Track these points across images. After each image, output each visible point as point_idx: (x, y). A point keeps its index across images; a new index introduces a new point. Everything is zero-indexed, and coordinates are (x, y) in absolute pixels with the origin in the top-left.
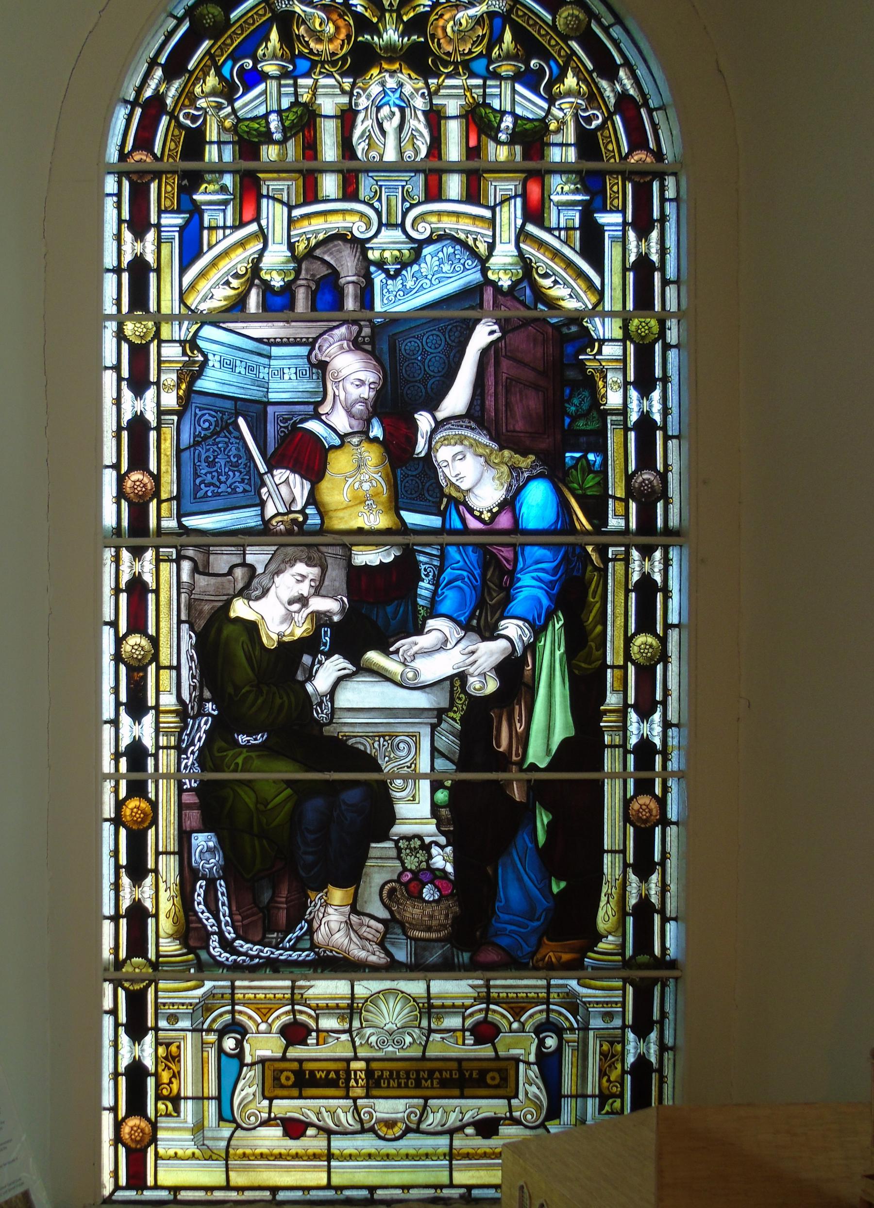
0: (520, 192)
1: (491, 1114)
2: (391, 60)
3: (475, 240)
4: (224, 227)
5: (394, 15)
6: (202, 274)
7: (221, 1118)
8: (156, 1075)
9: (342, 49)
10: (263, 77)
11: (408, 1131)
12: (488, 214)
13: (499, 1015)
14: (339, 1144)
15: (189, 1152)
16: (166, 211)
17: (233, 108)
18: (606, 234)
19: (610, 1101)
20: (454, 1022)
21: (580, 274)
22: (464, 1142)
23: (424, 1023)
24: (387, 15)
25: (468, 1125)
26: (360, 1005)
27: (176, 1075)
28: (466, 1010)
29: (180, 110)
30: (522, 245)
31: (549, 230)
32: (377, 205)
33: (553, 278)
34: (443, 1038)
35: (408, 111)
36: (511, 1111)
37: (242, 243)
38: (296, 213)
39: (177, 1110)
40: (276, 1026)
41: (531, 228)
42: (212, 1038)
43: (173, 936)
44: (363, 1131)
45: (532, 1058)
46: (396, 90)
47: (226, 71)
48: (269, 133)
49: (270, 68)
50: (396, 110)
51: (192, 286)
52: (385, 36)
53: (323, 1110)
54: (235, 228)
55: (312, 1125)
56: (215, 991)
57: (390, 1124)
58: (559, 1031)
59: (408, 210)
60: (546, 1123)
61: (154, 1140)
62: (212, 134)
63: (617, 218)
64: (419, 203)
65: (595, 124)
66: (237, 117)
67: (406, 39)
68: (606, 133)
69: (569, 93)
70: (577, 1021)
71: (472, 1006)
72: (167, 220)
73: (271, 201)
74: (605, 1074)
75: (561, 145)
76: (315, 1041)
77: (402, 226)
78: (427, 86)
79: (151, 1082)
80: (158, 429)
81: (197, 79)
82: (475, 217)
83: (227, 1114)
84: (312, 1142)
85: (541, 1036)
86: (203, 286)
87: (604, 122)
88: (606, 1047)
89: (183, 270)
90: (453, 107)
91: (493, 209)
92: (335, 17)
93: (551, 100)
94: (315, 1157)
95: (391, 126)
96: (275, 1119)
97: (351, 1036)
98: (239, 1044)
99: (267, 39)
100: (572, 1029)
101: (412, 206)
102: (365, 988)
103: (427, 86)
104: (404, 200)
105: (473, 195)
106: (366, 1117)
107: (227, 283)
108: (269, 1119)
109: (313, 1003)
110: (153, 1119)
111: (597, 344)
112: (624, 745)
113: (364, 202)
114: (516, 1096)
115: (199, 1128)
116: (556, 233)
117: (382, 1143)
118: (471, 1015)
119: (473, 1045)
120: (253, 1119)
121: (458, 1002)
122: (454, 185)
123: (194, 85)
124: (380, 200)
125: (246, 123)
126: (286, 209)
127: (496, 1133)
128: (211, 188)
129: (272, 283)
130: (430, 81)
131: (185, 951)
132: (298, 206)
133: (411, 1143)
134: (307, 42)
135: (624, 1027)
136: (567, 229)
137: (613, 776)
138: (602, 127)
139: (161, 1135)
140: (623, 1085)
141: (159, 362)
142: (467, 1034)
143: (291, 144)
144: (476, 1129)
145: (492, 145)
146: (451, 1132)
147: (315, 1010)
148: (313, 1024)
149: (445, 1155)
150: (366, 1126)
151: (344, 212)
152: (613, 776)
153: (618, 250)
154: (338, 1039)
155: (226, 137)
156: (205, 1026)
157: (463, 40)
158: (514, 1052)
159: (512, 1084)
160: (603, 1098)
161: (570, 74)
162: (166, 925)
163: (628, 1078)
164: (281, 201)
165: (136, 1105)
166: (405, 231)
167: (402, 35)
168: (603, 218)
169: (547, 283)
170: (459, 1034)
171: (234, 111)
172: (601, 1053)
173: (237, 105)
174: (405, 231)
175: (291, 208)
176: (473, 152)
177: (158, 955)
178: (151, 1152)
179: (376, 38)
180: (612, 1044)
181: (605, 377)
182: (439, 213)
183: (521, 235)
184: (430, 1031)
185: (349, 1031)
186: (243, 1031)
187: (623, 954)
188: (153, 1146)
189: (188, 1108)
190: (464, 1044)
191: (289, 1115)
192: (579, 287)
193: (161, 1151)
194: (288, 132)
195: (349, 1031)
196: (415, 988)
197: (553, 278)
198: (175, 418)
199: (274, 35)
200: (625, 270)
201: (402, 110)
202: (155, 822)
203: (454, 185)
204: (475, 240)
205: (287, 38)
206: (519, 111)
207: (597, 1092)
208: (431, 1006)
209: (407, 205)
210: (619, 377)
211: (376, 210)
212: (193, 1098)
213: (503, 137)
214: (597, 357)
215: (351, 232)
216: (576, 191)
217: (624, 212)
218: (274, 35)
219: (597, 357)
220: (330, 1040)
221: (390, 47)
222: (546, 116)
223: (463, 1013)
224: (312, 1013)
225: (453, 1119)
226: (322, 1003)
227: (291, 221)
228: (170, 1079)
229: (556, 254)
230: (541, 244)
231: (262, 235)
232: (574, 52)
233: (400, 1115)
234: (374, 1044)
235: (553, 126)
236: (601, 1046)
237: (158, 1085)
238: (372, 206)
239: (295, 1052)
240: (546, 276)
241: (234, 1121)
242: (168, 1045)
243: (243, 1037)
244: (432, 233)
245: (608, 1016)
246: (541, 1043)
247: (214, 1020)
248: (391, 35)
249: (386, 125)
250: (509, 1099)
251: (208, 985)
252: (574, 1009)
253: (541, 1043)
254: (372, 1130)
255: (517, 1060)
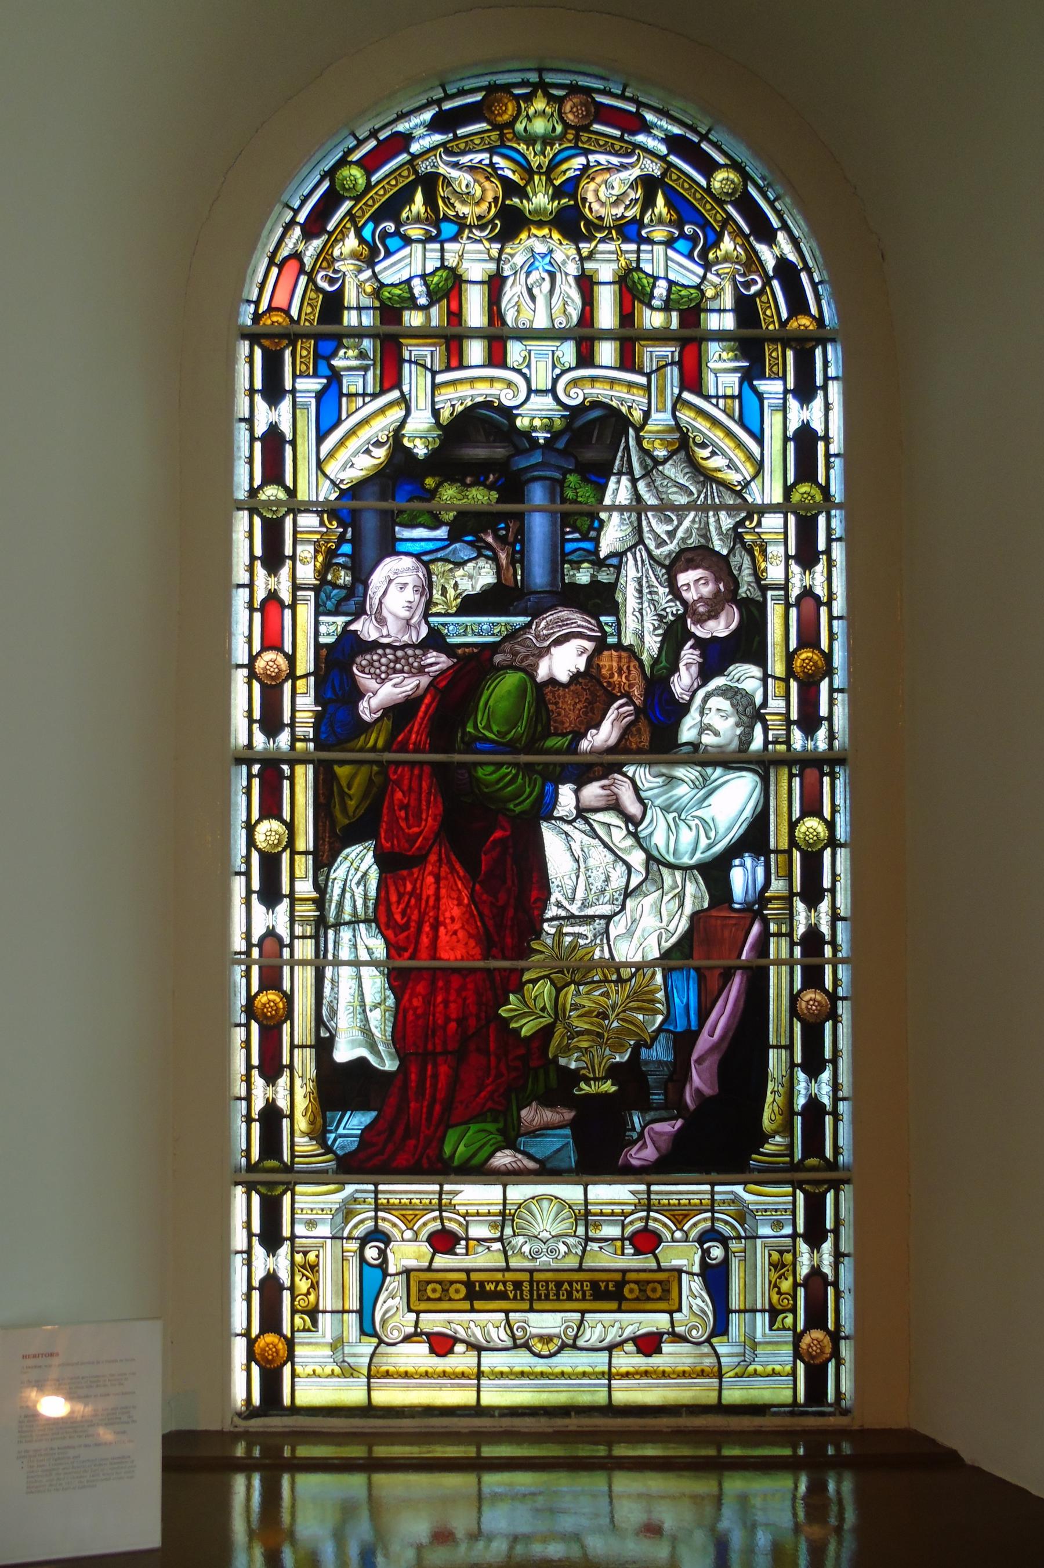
0: (677, 359)
1: (654, 1329)
2: (540, 224)
3: (630, 407)
4: (364, 395)
5: (544, 178)
6: (342, 443)
7: (363, 1332)
8: (292, 1288)
9: (489, 212)
10: (408, 241)
11: (563, 1347)
12: (643, 380)
13: (660, 1222)
14: (490, 1361)
15: (328, 1370)
16: (301, 376)
17: (374, 272)
18: (766, 402)
19: (781, 1316)
20: (614, 1231)
21: (740, 444)
22: (627, 1360)
23: (581, 1231)
24: (536, 178)
25: (625, 1341)
26: (513, 1211)
27: (314, 1286)
28: (626, 1217)
29: (318, 272)
30: (677, 414)
31: (707, 398)
32: (525, 371)
33: (710, 449)
34: (601, 1248)
35: (558, 275)
36: (673, 1327)
37: (382, 410)
38: (440, 378)
39: (315, 1322)
40: (424, 1234)
41: (686, 395)
42: (353, 1246)
43: (310, 1135)
44: (516, 1347)
45: (696, 1269)
46: (546, 255)
47: (367, 233)
48: (413, 298)
49: (415, 232)
50: (546, 276)
51: (331, 454)
52: (534, 200)
53: (472, 1324)
54: (375, 396)
55: (463, 1341)
56: (357, 1195)
57: (546, 1339)
58: (724, 1241)
59: (559, 376)
60: (714, 1340)
61: (291, 1357)
62: (351, 297)
63: (777, 386)
64: (570, 369)
65: (754, 289)
66: (378, 280)
67: (556, 202)
68: (764, 298)
69: (727, 259)
70: (745, 1230)
71: (632, 1214)
72: (302, 384)
73: (413, 366)
74: (775, 1286)
75: (720, 311)
76: (464, 1251)
77: (553, 391)
78: (578, 250)
79: (286, 1295)
80: (293, 607)
81: (336, 241)
82: (630, 385)
83: (368, 1329)
84: (461, 1360)
85: (705, 1246)
86: (343, 455)
87: (763, 289)
88: (776, 1256)
89: (320, 439)
90: (606, 272)
91: (648, 376)
92: (482, 180)
93: (707, 266)
94: (463, 1375)
95: (541, 292)
96: (422, 1334)
97: (503, 1245)
98: (383, 1253)
99: (411, 201)
100: (739, 1238)
101: (564, 372)
102: (518, 1193)
103: (578, 250)
104: (554, 367)
105: (627, 361)
106: (519, 1334)
107: (368, 452)
108: (416, 1334)
109: (462, 1210)
110: (289, 1335)
111: (756, 516)
112: (790, 934)
113: (514, 369)
114: (680, 1310)
115: (337, 1344)
116: (714, 401)
117: (537, 1360)
118: (631, 1223)
119: (633, 1255)
120: (396, 1333)
121: (617, 1209)
122: (607, 352)
123: (332, 246)
124: (529, 366)
125: (389, 289)
126: (429, 375)
127: (659, 1351)
128: (350, 353)
129: (415, 451)
130: (581, 245)
131: (322, 1151)
132: (441, 372)
133: (566, 1361)
134: (453, 205)
135: (794, 1236)
136: (725, 397)
137: (779, 962)
138: (761, 293)
139: (299, 1351)
140: (795, 1298)
141: (295, 532)
142: (627, 1243)
143: (434, 311)
144: (636, 1345)
145: (647, 312)
146: (610, 1349)
147: (464, 1217)
148: (461, 1232)
149: (603, 1373)
150: (519, 1342)
151: (492, 380)
152: (779, 962)
153: (778, 417)
154: (488, 1248)
155: (366, 301)
156: (345, 1234)
157: (615, 204)
158: (676, 1262)
159: (674, 1294)
160: (774, 1313)
161: (726, 238)
162: (302, 1123)
163: (801, 1292)
164: (424, 366)
165: (271, 1321)
166: (556, 398)
167: (553, 199)
168: (763, 386)
169: (705, 453)
170: (619, 1244)
171: (375, 275)
172: (770, 1264)
173: (377, 268)
174: (556, 398)
175: (434, 373)
176: (626, 317)
177: (293, 1156)
178: (287, 1370)
179: (525, 201)
180: (781, 1253)
181: (765, 550)
182: (593, 379)
183: (678, 400)
184: (588, 1239)
185: (500, 1239)
186: (387, 1239)
187: (791, 1155)
188: (289, 1364)
189: (325, 1321)
190: (623, 1254)
191: (436, 1330)
192: (738, 457)
193: (299, 1369)
194: (434, 296)
195: (500, 1239)
196: (572, 1193)
197: (710, 449)
198: (312, 594)
199: (419, 197)
200: (786, 440)
201: (552, 275)
202: (289, 1015)
203: (607, 352)
204: (630, 407)
205: (430, 201)
206: (672, 276)
207: (767, 1307)
208: (588, 1213)
209: (557, 371)
210: (781, 549)
211: (524, 375)
212: (332, 1312)
213: (656, 303)
214: (757, 530)
215: (499, 399)
216: (736, 359)
217: (784, 378)
218: (419, 197)
219: (757, 530)
220: (480, 1249)
221: (537, 211)
222: (701, 283)
223: (623, 1221)
224: (461, 1219)
225: (612, 1335)
226: (472, 1210)
227: (434, 386)
228: (308, 1290)
229: (715, 422)
230: (701, 412)
231: (404, 401)
232: (730, 217)
233: (556, 1331)
234: (527, 1253)
235: (710, 293)
236: (770, 1255)
237: (293, 1299)
238: (519, 371)
239: (442, 1261)
240: (703, 446)
241: (375, 1335)
242: (305, 1253)
243: (386, 1248)
244: (585, 399)
245: (778, 1224)
246: (706, 1253)
247: (355, 1227)
248: (540, 200)
249: (536, 291)
250: (671, 1313)
251: (350, 1189)
252: (741, 1218)
253: (706, 1253)
254: (526, 1346)
255: (679, 1271)
